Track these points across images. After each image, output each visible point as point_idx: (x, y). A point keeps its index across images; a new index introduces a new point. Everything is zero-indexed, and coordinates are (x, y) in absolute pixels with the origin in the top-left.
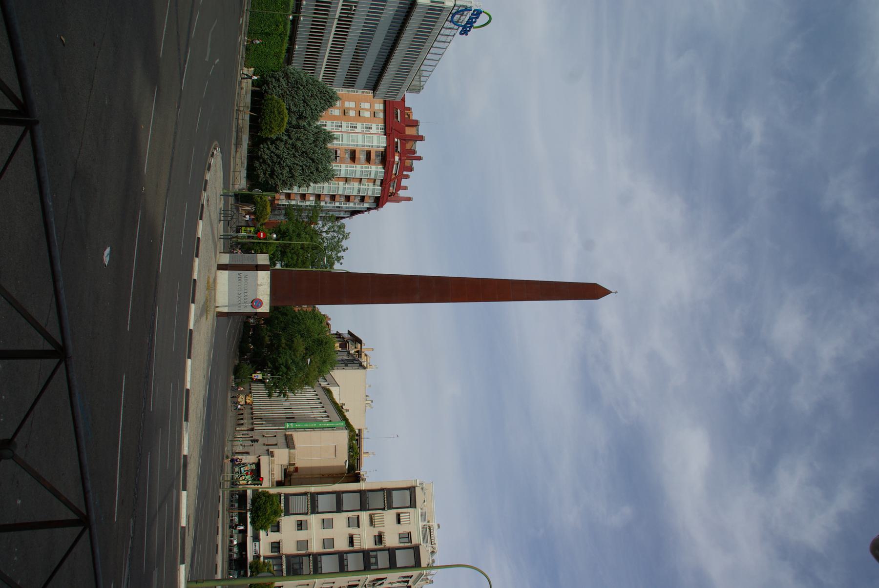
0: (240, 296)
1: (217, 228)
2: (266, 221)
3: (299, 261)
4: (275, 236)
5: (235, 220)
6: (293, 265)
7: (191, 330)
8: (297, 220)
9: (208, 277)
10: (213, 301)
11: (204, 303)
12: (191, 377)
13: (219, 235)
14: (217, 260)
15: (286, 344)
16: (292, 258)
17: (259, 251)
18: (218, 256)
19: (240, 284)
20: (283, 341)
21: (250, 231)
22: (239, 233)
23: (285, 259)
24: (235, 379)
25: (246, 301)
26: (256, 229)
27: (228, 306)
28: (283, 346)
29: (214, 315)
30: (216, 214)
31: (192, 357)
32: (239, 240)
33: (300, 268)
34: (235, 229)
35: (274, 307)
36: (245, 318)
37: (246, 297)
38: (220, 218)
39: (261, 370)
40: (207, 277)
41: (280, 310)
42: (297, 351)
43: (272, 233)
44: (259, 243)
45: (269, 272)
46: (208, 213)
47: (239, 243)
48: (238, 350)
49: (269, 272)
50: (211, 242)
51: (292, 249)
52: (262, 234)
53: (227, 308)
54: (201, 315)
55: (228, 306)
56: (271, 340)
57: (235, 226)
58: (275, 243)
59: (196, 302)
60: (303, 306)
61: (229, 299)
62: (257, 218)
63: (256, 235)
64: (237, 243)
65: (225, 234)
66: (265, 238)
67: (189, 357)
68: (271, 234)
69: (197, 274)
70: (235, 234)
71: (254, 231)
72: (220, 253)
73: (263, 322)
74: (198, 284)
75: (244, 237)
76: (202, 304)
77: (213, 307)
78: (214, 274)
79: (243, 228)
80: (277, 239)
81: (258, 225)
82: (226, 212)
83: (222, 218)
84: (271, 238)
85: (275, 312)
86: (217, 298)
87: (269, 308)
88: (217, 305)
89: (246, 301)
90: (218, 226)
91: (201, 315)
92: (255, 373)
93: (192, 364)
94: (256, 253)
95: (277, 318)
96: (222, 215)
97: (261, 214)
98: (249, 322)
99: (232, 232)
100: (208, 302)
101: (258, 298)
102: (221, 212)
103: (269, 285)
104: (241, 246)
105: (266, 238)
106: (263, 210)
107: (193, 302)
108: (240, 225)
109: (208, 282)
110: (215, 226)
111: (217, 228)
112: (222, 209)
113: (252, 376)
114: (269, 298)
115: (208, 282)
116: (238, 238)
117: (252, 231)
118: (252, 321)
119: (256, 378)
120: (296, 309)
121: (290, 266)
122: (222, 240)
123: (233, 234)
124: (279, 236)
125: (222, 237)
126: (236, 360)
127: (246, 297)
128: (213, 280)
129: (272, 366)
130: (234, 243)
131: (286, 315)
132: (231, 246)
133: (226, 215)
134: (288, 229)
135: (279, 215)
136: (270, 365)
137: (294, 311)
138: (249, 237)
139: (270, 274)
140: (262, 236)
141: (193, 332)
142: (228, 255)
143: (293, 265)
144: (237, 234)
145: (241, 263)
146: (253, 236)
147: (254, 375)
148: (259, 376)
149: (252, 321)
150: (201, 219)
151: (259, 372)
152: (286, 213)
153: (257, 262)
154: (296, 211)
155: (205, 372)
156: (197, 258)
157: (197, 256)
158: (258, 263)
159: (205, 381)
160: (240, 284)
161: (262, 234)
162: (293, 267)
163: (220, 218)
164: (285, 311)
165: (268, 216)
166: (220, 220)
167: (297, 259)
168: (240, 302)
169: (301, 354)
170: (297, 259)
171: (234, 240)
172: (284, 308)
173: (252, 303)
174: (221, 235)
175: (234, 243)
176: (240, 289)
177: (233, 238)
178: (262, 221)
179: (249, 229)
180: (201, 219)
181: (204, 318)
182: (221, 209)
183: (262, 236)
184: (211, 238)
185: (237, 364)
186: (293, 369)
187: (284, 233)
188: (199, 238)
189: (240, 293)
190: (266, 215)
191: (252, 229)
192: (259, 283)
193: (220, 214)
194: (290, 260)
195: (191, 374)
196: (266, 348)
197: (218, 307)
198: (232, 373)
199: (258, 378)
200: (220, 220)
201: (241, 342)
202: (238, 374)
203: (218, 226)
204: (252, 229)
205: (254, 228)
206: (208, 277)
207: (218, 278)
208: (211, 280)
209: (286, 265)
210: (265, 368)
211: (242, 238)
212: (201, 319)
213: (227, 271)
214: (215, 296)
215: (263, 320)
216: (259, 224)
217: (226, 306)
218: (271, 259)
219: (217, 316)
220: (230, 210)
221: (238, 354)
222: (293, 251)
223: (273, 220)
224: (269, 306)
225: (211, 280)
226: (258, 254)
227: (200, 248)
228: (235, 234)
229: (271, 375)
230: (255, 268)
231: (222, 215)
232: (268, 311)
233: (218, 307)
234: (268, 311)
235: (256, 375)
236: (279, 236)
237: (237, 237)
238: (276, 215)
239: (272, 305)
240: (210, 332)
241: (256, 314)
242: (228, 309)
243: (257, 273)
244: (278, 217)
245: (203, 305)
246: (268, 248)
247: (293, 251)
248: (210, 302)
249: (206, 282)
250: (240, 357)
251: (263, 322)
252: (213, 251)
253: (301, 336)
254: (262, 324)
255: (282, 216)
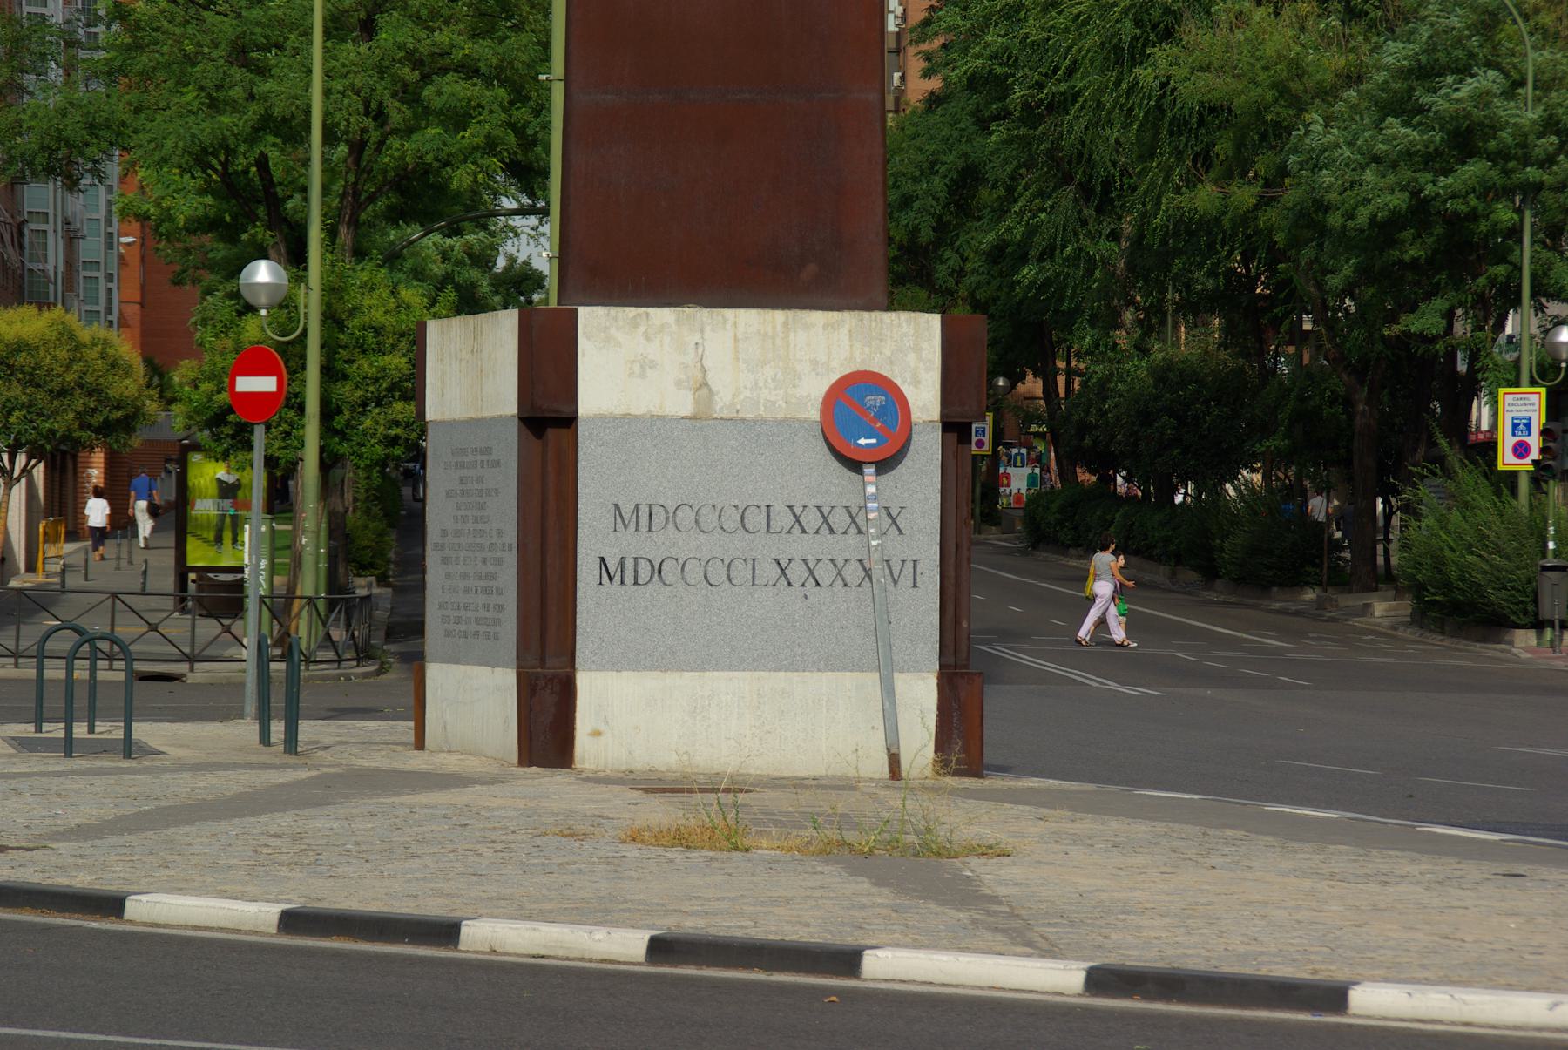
0: (797, 572)
1: (198, 768)
2: (126, 349)
3: (485, 52)
4: (263, 273)
5: (128, 629)
6: (521, 114)
7: (1099, 980)
8: (112, 73)
9: (635, 837)
10: (844, 803)
11: (855, 872)
12: (1510, 987)
13: (265, 756)
14: (472, 765)
15: (1238, 167)
16: (458, 119)
17: (400, 409)
18: (451, 763)
19: (694, 572)
20: (1205, 197)
21: (227, 491)
22: (239, 586)
23: (460, 178)
24: (1539, 625)
25: (840, 519)
26: (204, 436)
27: (886, 670)
28: (1244, 195)
29: (954, 792)
30: (68, 783)
31: (1333, 972)
32: (310, 583)
33: (546, 46)
34: (208, 628)
35: (898, 280)
36: (993, 535)
37: (812, 520)
38: (102, 748)
39: (1463, 392)
40: (632, 851)
41: (926, 235)
42: (1298, 69)
43: (236, 295)
44: (328, 412)
45: (583, 311)
46: (62, 846)
47: (335, 585)
48: (1279, 601)
49: (583, 311)
50: (319, 823)
51: (380, 116)
52: (245, 384)
53: (902, 681)
54: (966, 895)
55: (886, 670)
56: (1194, 308)
57: (177, 626)
58: (329, 269)
59: (850, 939)
60: (892, 26)
61: (830, 663)
62: (106, 429)
63: (259, 436)
64: (331, 605)
65: (251, 706)
66: (288, 358)
67: (1334, 997)
68: (251, 309)
69: (600, 934)
70: (252, 625)
71: (225, 456)
72: (420, 744)
73: (1032, 385)
74: (691, 924)
75: (282, 551)
76: (864, 885)
77: (894, 799)
78: (602, 791)
79: (199, 554)
80: (296, 257)
81: (176, 423)
82: (55, 702)
83: (110, 730)
84: (286, 305)
85: (941, 272)
86: (820, 771)
87: (904, 316)
88: (878, 766)
89: (840, 519)
90: (180, 767)
91: (966, 895)
92: (1489, 448)
93: (1395, 975)
94: (419, 424)
95: (1003, 257)
96: (80, 730)
97: (63, 393)
98: (1034, 506)
99: (233, 651)
100: (851, 836)
101: (815, 415)
102: (48, 745)
103: (704, 314)
104: (363, 568)
105: (283, 348)
106: (32, 381)
107: (847, 960)
108: (169, 583)
109: (680, 839)
110: (182, 787)
111: (198, 768)
112: (27, 730)
113: (1514, 475)
114: (818, 317)
115: (680, 839)
116: (290, 596)
117: (220, 471)
118: (1018, 480)
119: (1534, 441)
120: (919, 88)
121: (532, 141)
122: (308, 729)
123: (250, 640)
124: (260, 232)
125: (278, 728)
126: (1366, 609)
127: (812, 520)
128: (655, 801)
129: (1439, 304)
130: (338, 634)
131: (969, 178)
132: (364, 653)
133: (81, 701)
134: (200, 158)
135: (72, 239)
136: (1424, 321)
137: (934, 101)
138: (280, 498)
139: (599, 311)
140: (267, 384)
141: (1112, 959)
142: (437, 674)
143: (521, 114)
144: (251, 604)
145: (511, 559)
146: (270, 462)
147: (1507, 459)
148: (1522, 412)
149: (1018, 480)
150: (112, 905)
151: (1481, 414)
152: (50, 171)
153: (501, 420)
154: (29, 80)
155: (1473, 871)
156: (464, 930)
157: (447, 932)
158: (510, 407)
159: (1544, 872)
160: (694, 572)
161: (245, 384)
162: (541, 109)
163: (102, 748)
164: (938, 183)
165: (85, 335)
166: (128, 748)
167: (469, 70)
168: (853, 573)
169: (1326, 39)
170: (469, 70)
171: (303, 629)
172: (906, 202)
173: (855, 466)
174: (265, 738)
175: (338, 634)
176: (741, 572)
177: (285, 641)
178: (129, 386)
179: (205, 508)
180: (112, 905)
181: (992, 875)
182: (23, 744)
183: (267, 384)
184: (285, 821)
185: (1406, 606)
186: (1482, 98)
187: (229, 187)
188: (291, 921)
189: (770, 572)
190: (78, 347)
191: (207, 473)
192: (681, 404)
193: (69, 746)
194: (472, 135)
195: (1492, 984)
196: (1262, 353)
197: (894, 761)
198: (1493, 650)
199: (1538, 418)
200: (128, 748)
201: (1210, 573)
202: (1494, 595)
203: (180, 767)
204: (207, 473)
205: (195, 458)
206: (635, 837)
207: (639, 765)
208: (660, 813)
209: (528, 175)
210: (1451, 357)
211: (284, 559)
212: (995, 899)
213: (587, 684)
214: (798, 784)
215: (1015, 378)
216: (151, 406)
217: (888, 691)
218: (470, 303)
219: (973, 766)
220: (31, 673)
221: (1310, 595)
222: (397, 113)
223: (126, 294)
224: (889, 317)
225: (660, 813)
226: (431, 414)
227: (376, 906)
228: (252, 625)
229: (1516, 303)
230: (551, 433)
231: (80, 730)
232: (934, 321)
233: (894, 761)
234: (934, 321)
235: (1507, 442)
236: (260, 232)
237: (280, 607)
238: (70, 264)
239: (882, 298)
240: (1115, 826)
241: (954, 428)
242: (915, 668)
243: (602, 419)
244: (90, 248)
245: (880, 882)
246: (378, 331)
247: (397, 113)
248: (846, 821)
249: (676, 854)
250: (1339, 580)
251: (1032, 385)
252: (407, 799)
253: (1167, 35)
254: (1050, 391)
255: (76, 204)
